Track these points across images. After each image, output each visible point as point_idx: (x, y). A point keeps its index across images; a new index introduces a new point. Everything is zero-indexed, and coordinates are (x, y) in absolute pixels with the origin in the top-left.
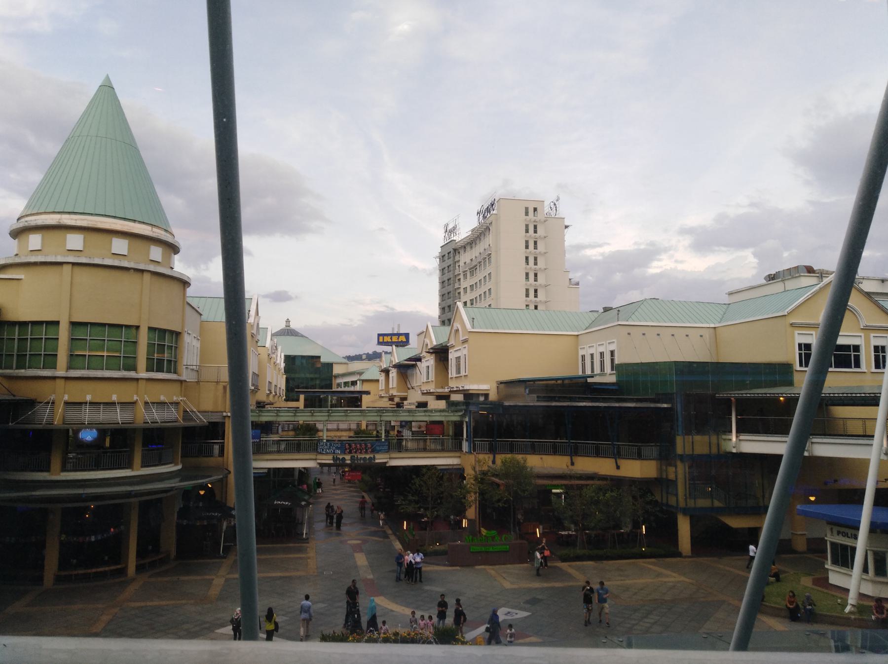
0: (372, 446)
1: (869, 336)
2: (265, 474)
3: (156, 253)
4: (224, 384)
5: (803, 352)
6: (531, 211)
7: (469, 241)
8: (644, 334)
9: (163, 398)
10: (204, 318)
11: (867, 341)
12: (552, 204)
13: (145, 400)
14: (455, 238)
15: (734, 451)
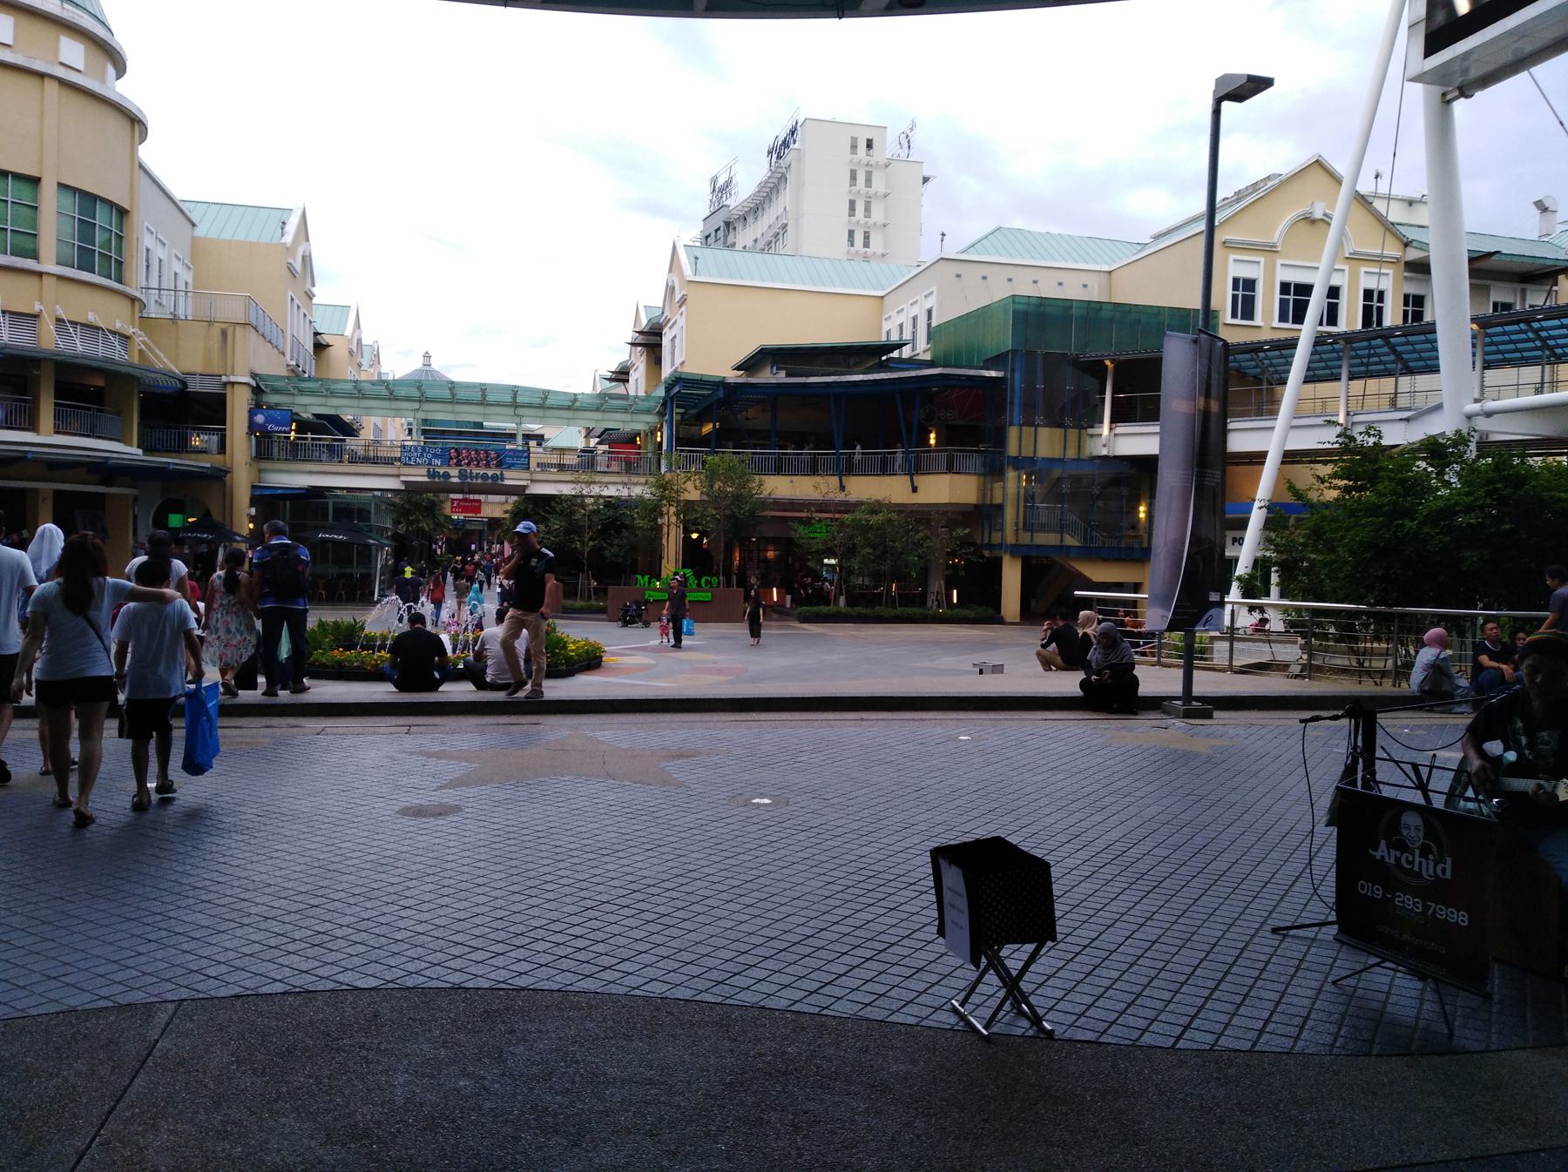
0: (498, 456)
1: (1358, 271)
2: (304, 491)
3: (72, 52)
4: (223, 326)
5: (1240, 293)
6: (862, 145)
7: (752, 205)
8: (984, 278)
9: (91, 318)
10: (200, 231)
11: (1354, 280)
12: (903, 136)
13: (58, 313)
14: (727, 203)
15: (1104, 452)
